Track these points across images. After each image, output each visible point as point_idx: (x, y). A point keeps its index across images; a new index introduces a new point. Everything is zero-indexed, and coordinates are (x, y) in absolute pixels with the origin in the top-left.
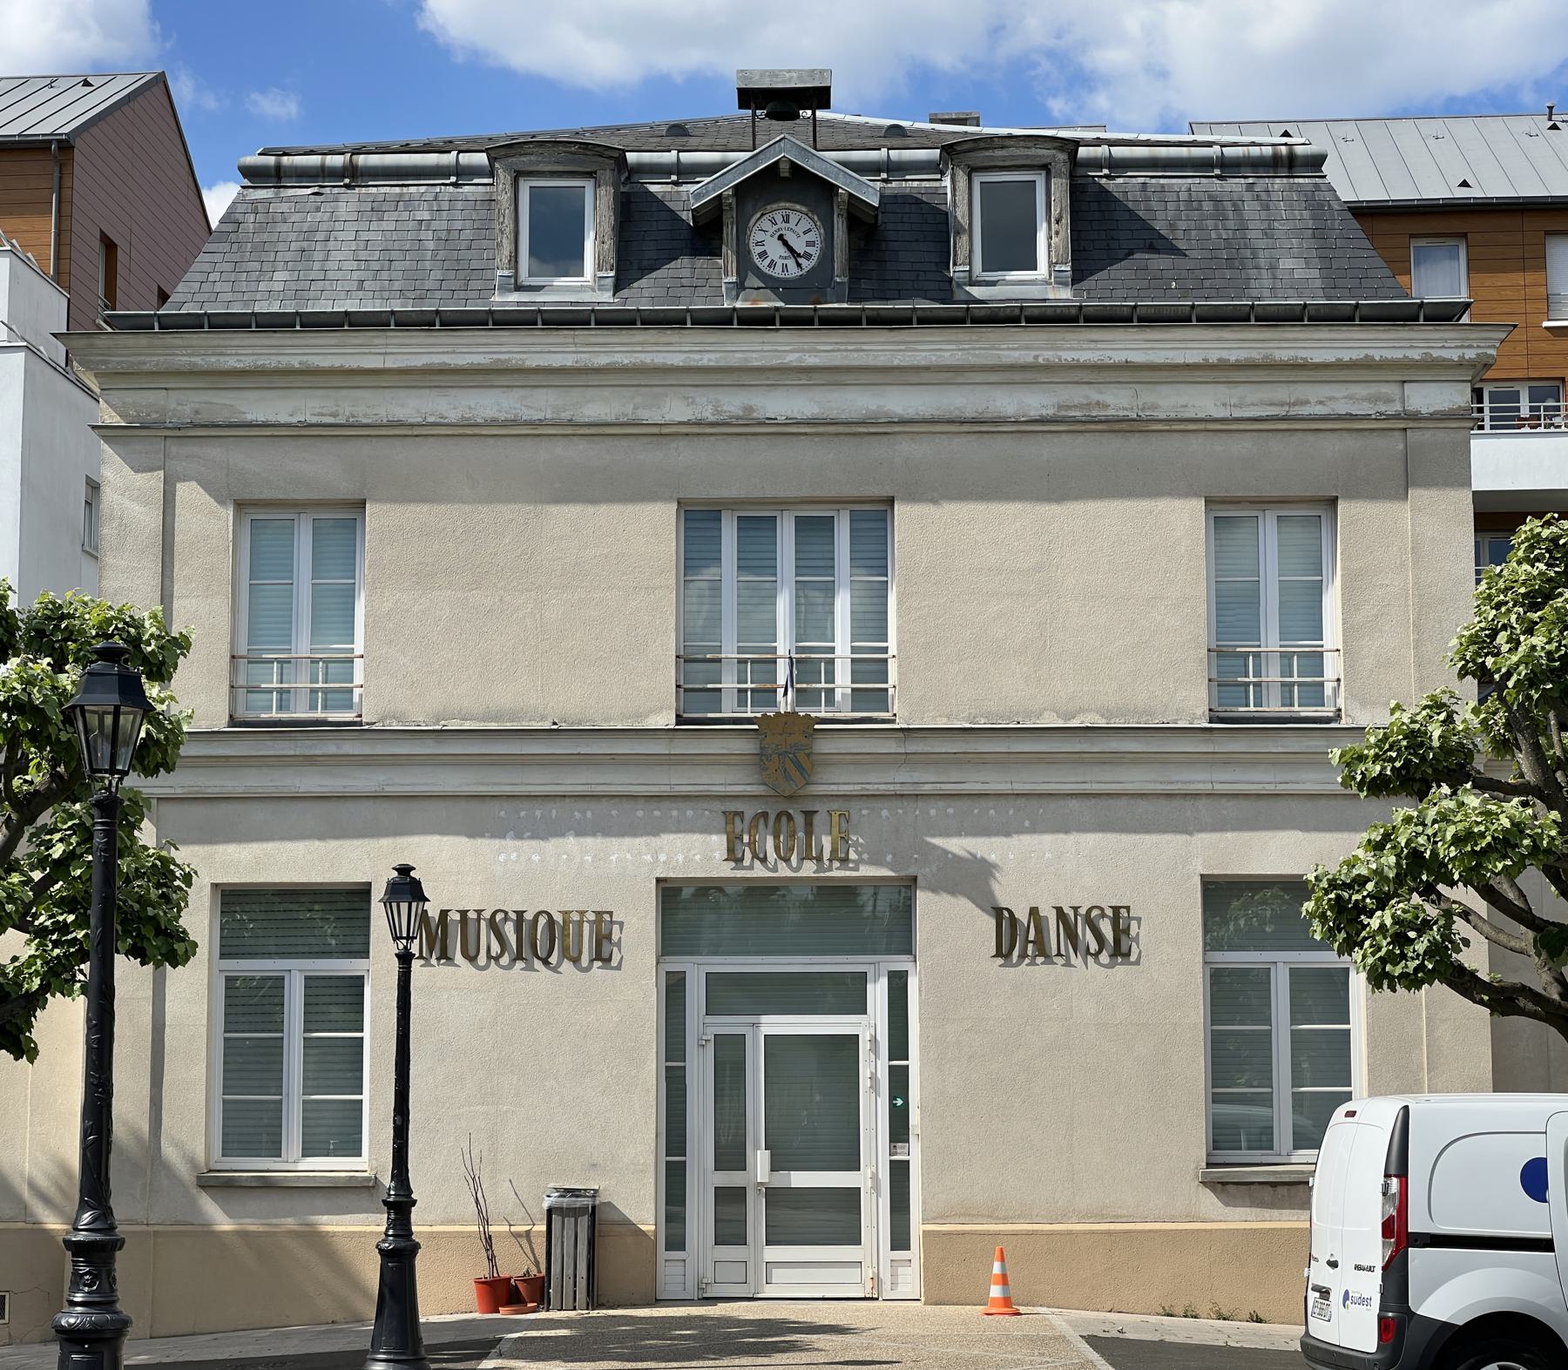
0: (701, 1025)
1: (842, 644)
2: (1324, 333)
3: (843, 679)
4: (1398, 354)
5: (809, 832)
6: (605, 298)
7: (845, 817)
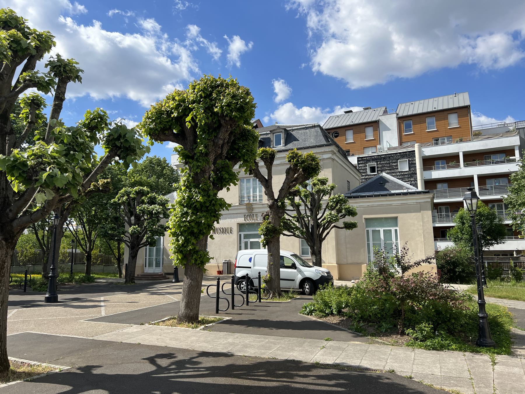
1: (258, 194)
2: (311, 149)
3: (258, 198)
6: (284, 148)
7: (440, 208)
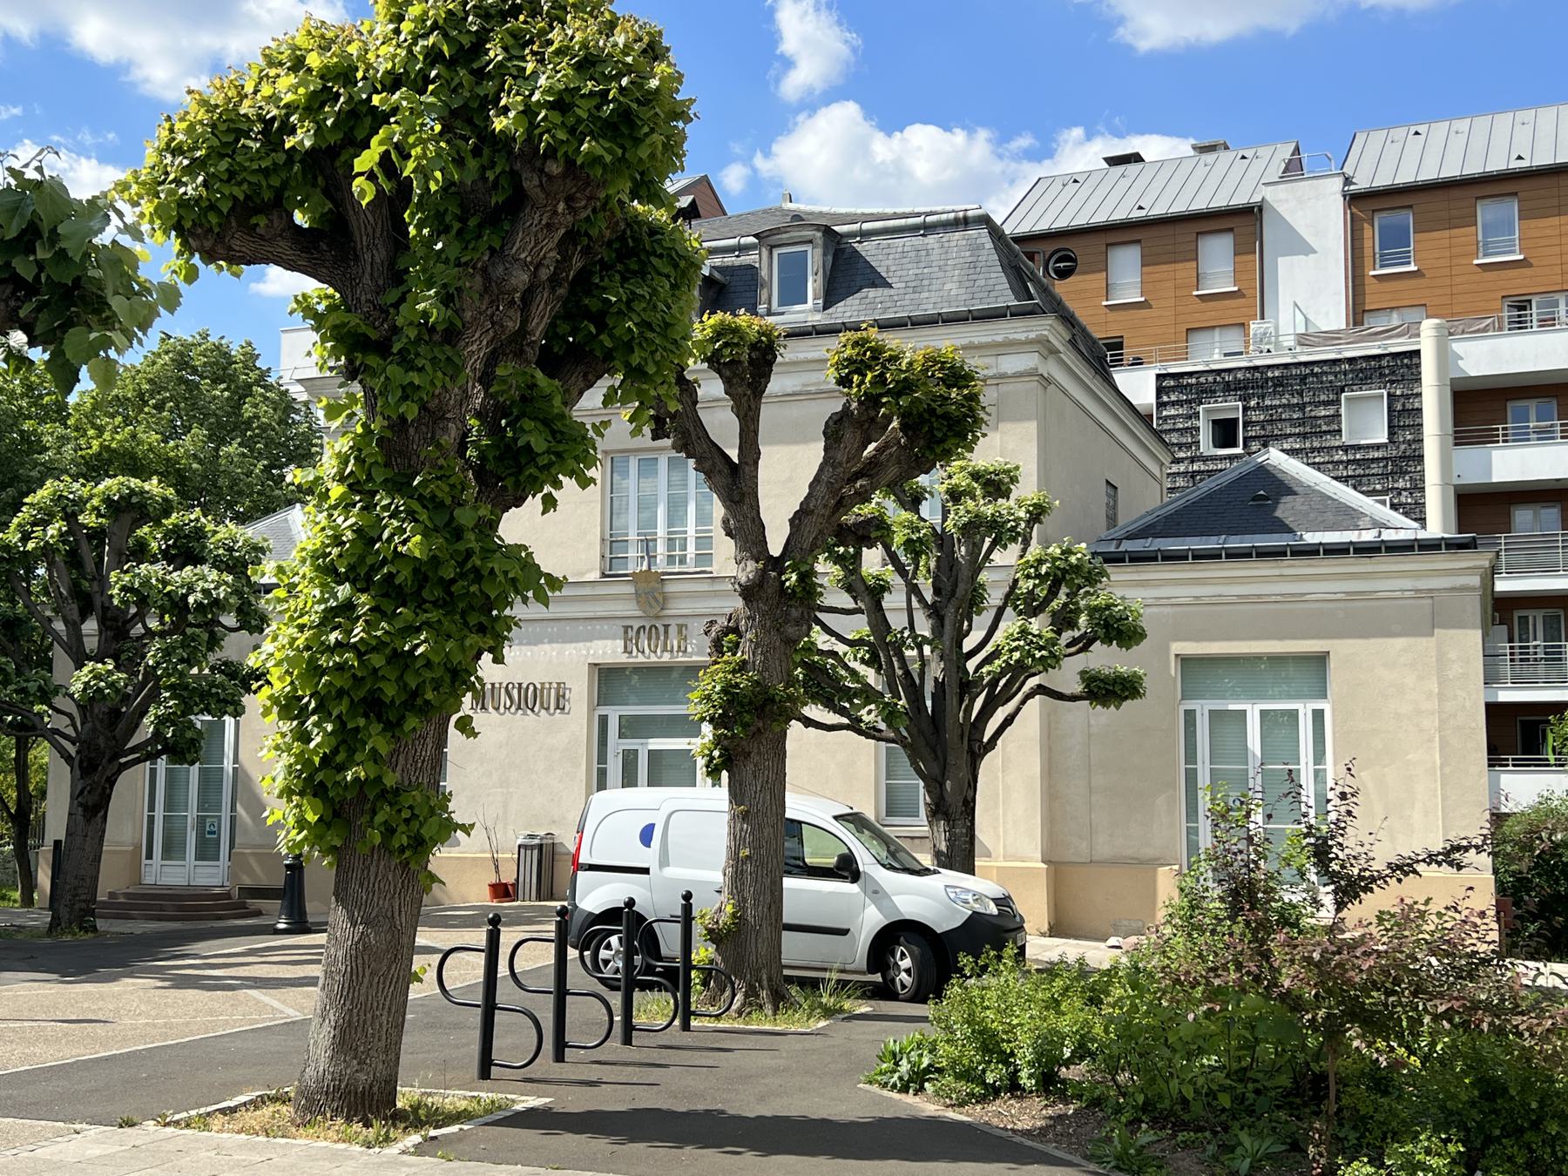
0: (616, 745)
1: (691, 530)
4: (989, 339)
5: (666, 637)
6: (818, 319)
